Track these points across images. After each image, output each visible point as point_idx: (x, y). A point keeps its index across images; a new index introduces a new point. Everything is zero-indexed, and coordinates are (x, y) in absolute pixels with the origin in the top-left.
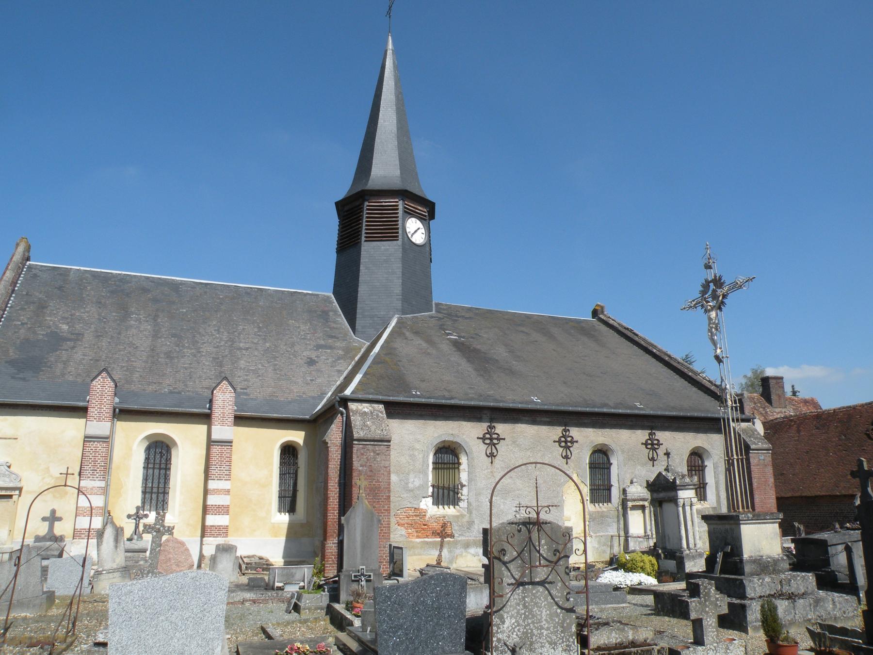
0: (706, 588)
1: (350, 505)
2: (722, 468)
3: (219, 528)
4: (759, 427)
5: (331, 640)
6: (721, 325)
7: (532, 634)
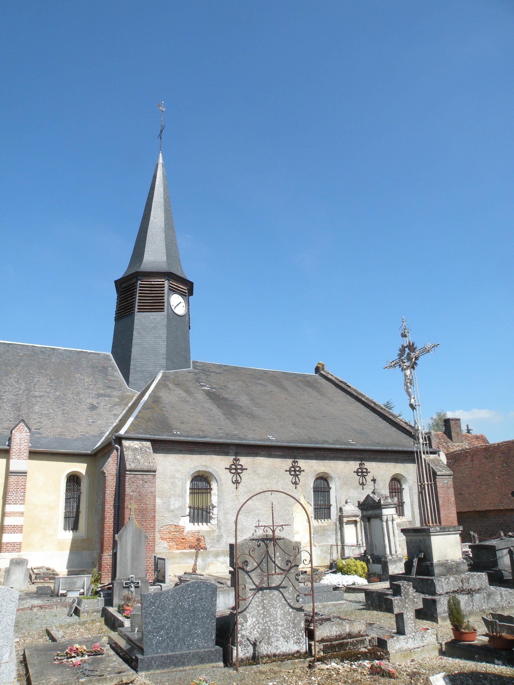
0: (405, 588)
1: (123, 524)
2: (416, 490)
3: (13, 544)
4: (443, 458)
5: (105, 639)
6: (414, 380)
7: (270, 630)
